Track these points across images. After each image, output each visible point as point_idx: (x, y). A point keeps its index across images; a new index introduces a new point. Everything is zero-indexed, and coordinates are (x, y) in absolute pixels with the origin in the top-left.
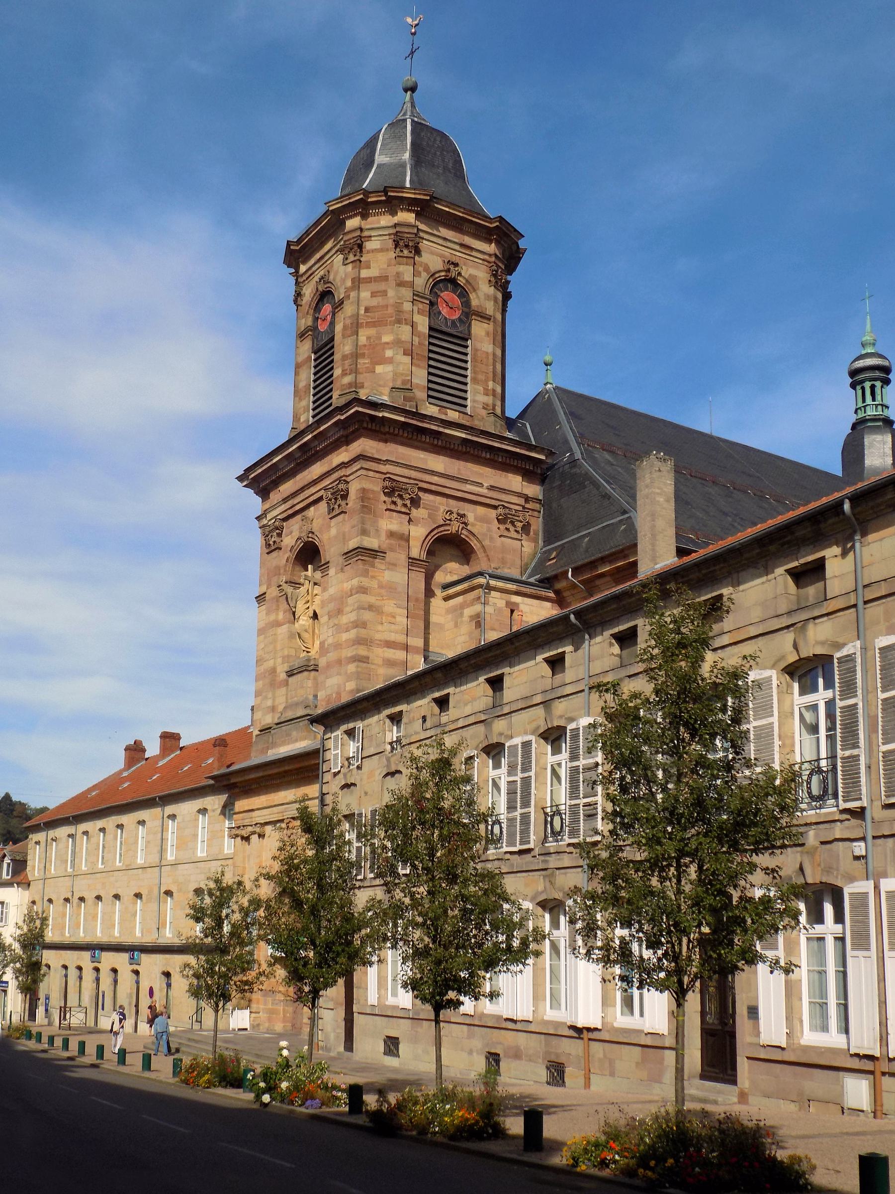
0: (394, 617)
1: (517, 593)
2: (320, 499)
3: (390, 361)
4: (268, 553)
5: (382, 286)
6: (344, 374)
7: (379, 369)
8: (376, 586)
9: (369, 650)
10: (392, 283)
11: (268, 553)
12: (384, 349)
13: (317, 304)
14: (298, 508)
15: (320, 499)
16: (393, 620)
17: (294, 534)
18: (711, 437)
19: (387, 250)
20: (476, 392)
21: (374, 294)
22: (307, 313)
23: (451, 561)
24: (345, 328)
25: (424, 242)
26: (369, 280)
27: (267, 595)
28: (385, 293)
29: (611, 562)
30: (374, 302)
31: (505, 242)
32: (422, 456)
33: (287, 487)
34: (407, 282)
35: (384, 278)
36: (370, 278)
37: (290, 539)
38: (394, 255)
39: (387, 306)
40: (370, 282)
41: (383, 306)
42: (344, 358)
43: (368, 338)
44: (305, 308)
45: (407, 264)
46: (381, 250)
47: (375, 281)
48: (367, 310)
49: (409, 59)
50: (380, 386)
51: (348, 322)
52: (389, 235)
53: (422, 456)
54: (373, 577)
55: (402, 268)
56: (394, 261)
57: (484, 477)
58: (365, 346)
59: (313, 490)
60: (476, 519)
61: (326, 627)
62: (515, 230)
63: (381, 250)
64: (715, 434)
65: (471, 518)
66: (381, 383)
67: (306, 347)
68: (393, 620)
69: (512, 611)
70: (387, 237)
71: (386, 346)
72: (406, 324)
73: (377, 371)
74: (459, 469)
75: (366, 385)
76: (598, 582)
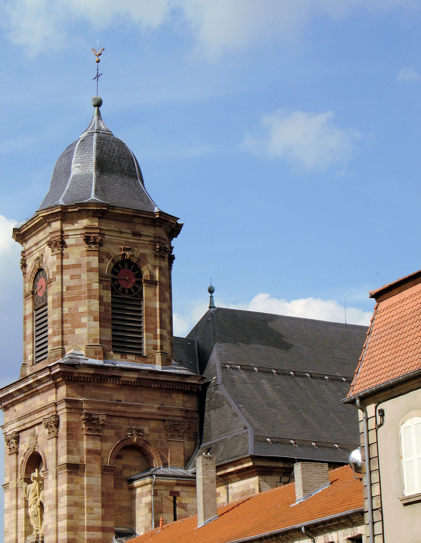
0: (92, 509)
1: (177, 485)
2: (41, 423)
3: (83, 325)
4: (9, 455)
5: (77, 271)
6: (54, 334)
7: (78, 331)
8: (79, 489)
9: (75, 534)
10: (84, 269)
11: (9, 455)
12: (80, 317)
13: (34, 283)
14: (28, 426)
15: (41, 423)
16: (91, 511)
17: (26, 443)
18: (346, 326)
19: (80, 245)
20: (148, 338)
21: (72, 277)
22: (30, 281)
23: (257, 294)
24: (53, 301)
25: (106, 237)
26: (69, 267)
27: (10, 485)
28: (79, 276)
29: (235, 466)
30: (72, 283)
31: (165, 224)
32: (109, 393)
33: (20, 408)
34: (93, 268)
35: (79, 266)
36: (69, 265)
37: (24, 447)
38: (86, 249)
39: (81, 286)
40: (69, 268)
41: (78, 286)
42: (54, 323)
43: (70, 309)
44: (28, 276)
45: (94, 256)
46: (76, 245)
47: (73, 268)
48: (68, 288)
49: (100, 73)
50: (79, 343)
51: (56, 297)
52: (81, 234)
53: (109, 393)
54: (77, 483)
55: (91, 258)
56: (85, 254)
57: (150, 404)
58: (67, 314)
59: (37, 416)
60: (150, 431)
61: (48, 515)
62: (172, 217)
63: (76, 245)
64: (348, 323)
65: (146, 430)
66: (80, 341)
67: (29, 306)
68: (91, 511)
69: (175, 498)
70: (79, 236)
71: (82, 314)
72: (95, 299)
73: (76, 333)
74: (136, 398)
75: (69, 342)
76: (230, 477)
